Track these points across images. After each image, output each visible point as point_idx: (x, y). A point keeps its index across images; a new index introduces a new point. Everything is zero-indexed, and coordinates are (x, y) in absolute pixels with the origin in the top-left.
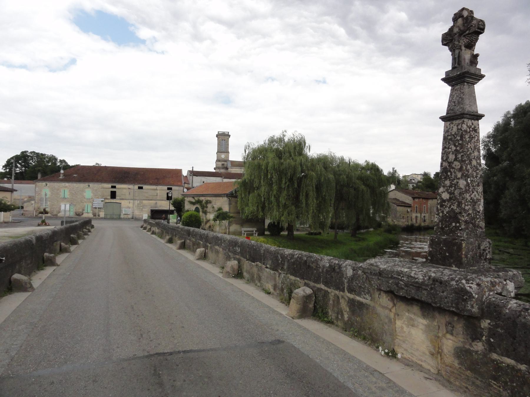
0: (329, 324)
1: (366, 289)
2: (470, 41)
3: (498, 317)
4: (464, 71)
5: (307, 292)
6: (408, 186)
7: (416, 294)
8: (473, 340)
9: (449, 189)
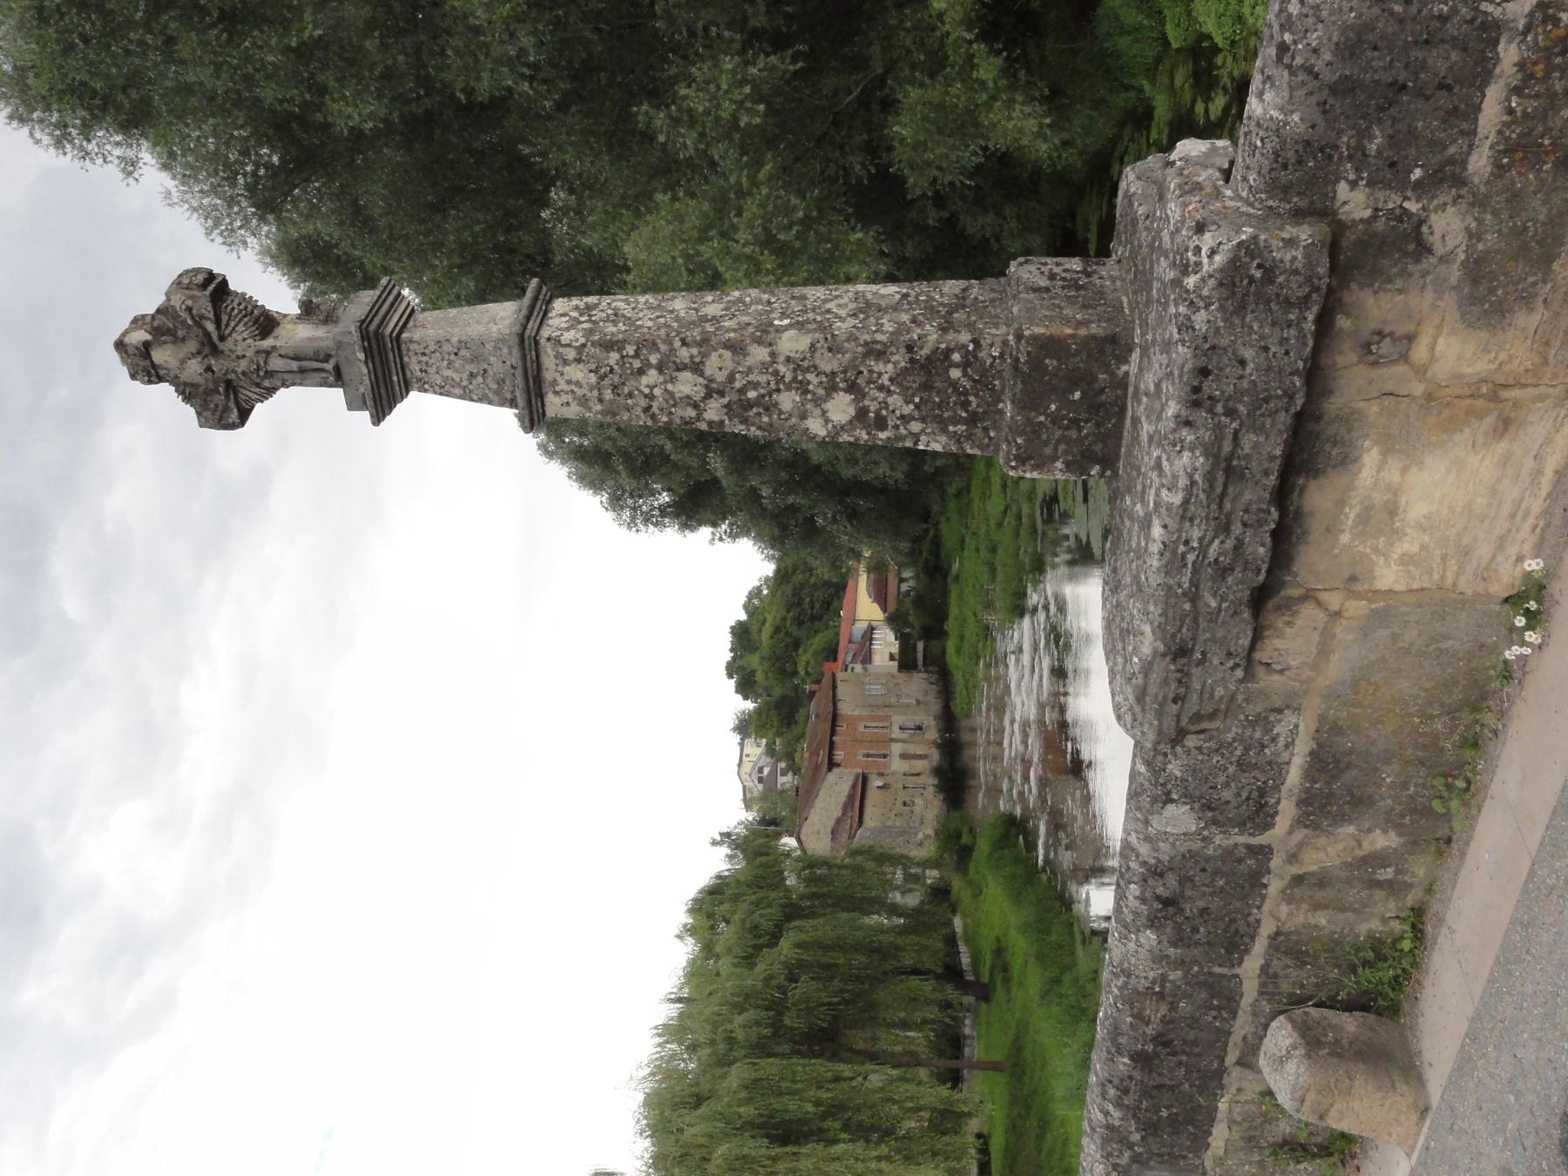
0: (1429, 928)
1: (1248, 733)
2: (245, 316)
3: (1321, 150)
4: (356, 336)
5: (1288, 1042)
6: (783, 791)
7: (1259, 481)
8: (1424, 249)
9: (814, 394)
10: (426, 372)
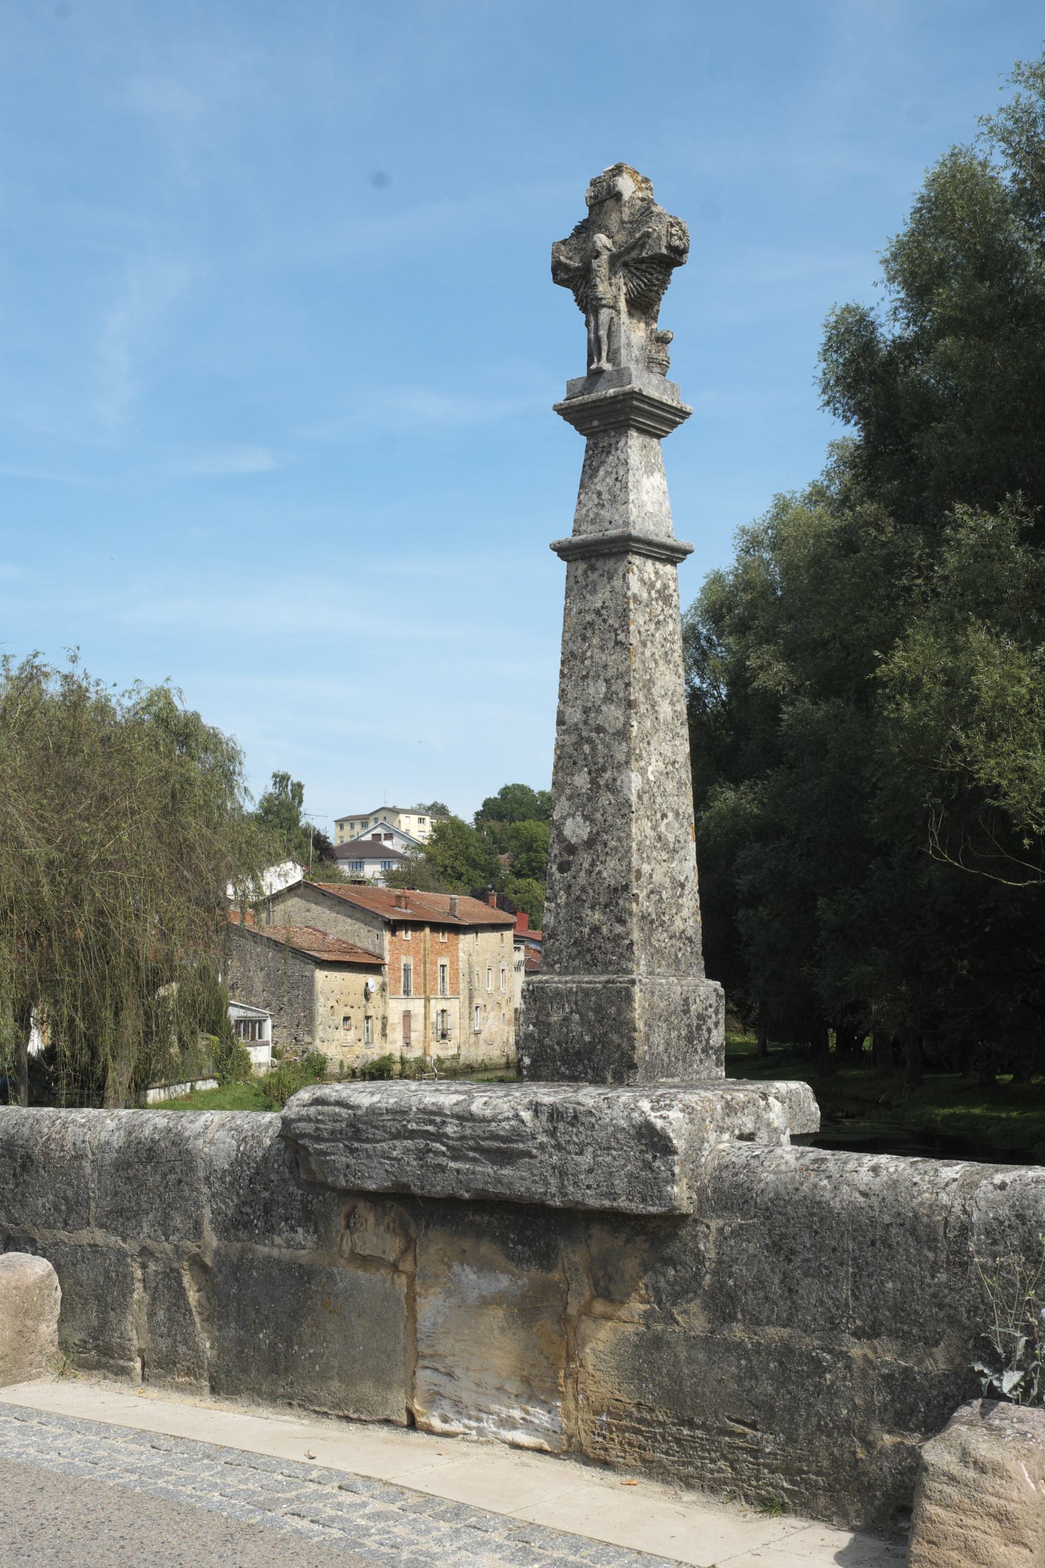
10: (603, 451)
